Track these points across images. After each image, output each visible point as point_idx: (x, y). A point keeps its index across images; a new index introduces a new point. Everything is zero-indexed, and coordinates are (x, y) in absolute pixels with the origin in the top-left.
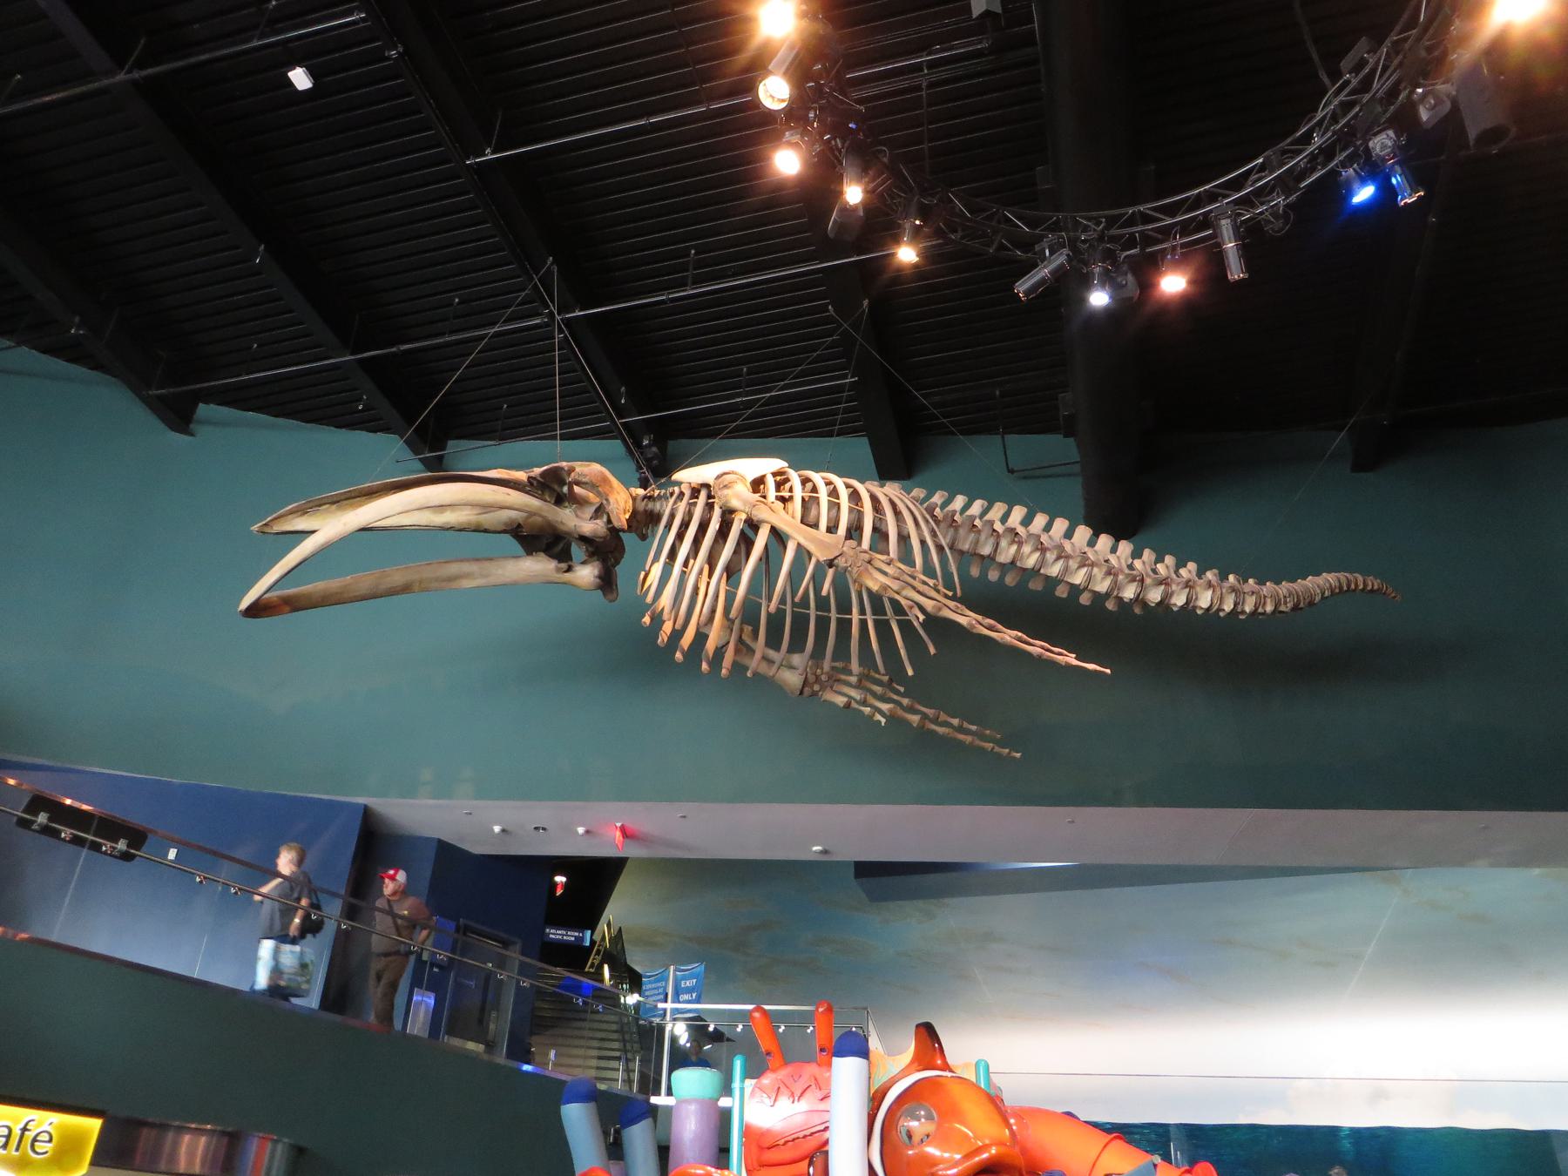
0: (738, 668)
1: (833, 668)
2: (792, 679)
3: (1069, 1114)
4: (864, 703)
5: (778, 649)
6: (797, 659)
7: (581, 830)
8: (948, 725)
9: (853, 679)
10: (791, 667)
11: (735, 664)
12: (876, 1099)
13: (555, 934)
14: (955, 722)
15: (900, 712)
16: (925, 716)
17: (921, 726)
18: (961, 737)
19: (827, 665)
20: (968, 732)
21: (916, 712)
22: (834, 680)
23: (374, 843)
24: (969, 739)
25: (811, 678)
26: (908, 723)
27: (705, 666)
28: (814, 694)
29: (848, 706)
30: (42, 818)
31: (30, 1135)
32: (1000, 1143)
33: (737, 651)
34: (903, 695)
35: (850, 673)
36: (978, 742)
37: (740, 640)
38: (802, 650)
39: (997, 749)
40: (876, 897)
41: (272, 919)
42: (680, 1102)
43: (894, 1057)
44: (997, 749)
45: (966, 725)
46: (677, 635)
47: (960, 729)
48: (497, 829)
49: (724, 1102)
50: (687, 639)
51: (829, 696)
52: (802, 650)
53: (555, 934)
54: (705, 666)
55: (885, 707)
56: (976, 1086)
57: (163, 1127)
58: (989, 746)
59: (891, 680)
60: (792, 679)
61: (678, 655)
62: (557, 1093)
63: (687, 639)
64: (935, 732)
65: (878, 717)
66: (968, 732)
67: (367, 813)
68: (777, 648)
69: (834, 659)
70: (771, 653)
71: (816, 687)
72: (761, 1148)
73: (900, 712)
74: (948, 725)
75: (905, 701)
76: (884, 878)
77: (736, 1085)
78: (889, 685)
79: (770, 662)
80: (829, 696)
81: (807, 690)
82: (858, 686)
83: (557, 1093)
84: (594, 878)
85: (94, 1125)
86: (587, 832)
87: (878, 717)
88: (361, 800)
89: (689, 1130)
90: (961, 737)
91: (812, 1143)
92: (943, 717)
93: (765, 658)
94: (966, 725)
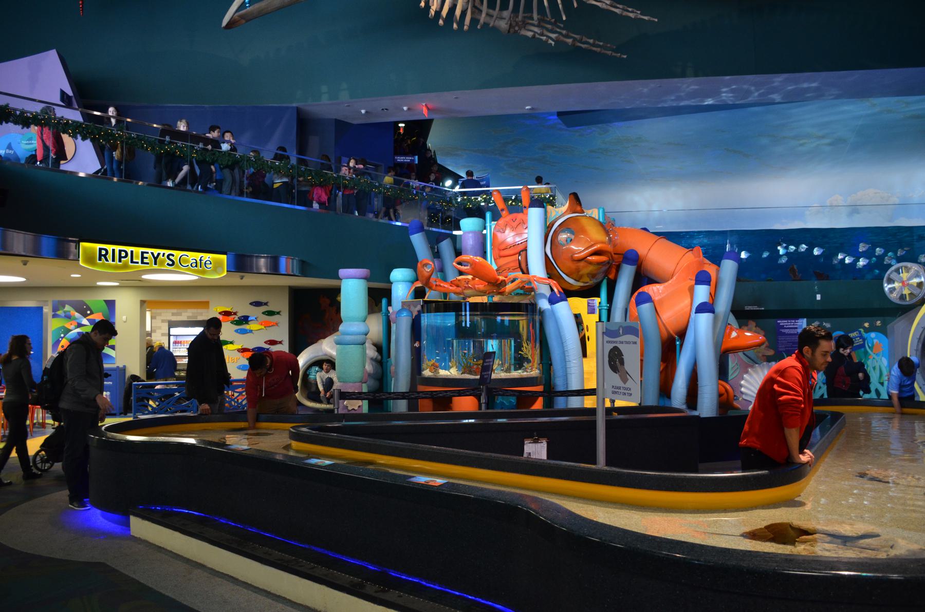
0: (474, 21)
1: (524, 17)
2: (503, 25)
3: (645, 229)
4: (542, 35)
5: (494, 9)
6: (506, 14)
7: (405, 108)
8: (588, 43)
9: (536, 23)
10: (502, 18)
11: (472, 20)
12: (548, 228)
13: (400, 159)
14: (591, 41)
15: (562, 38)
16: (575, 39)
17: (573, 45)
18: (594, 49)
19: (520, 18)
20: (599, 46)
21: (571, 37)
22: (524, 25)
23: (305, 124)
24: (598, 50)
25: (514, 24)
26: (566, 43)
27: (455, 26)
28: (516, 32)
29: (534, 37)
30: (168, 139)
31: (203, 262)
32: (602, 243)
33: (472, 13)
34: (563, 29)
35: (532, 19)
36: (603, 51)
37: (474, 6)
38: (507, 8)
39: (614, 54)
40: (569, 125)
41: (681, 345)
42: (465, 233)
43: (561, 211)
44: (614, 54)
45: (597, 42)
46: (438, 13)
47: (594, 45)
48: (363, 111)
49: (484, 232)
50: (444, 13)
51: (524, 32)
52: (507, 8)
53: (400, 159)
54: (455, 26)
55: (553, 36)
56: (594, 219)
57: (251, 257)
58: (609, 53)
59: (556, 21)
60: (503, 25)
61: (441, 22)
62: (405, 233)
63: (444, 13)
64: (581, 47)
65: (550, 41)
66: (599, 46)
67: (299, 111)
68: (494, 9)
69: (524, 12)
70: (491, 11)
71: (517, 28)
72: (500, 250)
73: (562, 38)
74: (588, 43)
75: (564, 32)
76: (572, 118)
77: (488, 225)
78: (555, 24)
79: (492, 16)
80: (524, 32)
81: (512, 30)
82: (538, 26)
83: (405, 233)
84: (420, 128)
85: (224, 257)
86: (409, 109)
87: (550, 41)
88: (294, 105)
89: (469, 242)
90: (594, 49)
91: (522, 247)
92: (585, 39)
93: (487, 14)
94: (597, 42)
